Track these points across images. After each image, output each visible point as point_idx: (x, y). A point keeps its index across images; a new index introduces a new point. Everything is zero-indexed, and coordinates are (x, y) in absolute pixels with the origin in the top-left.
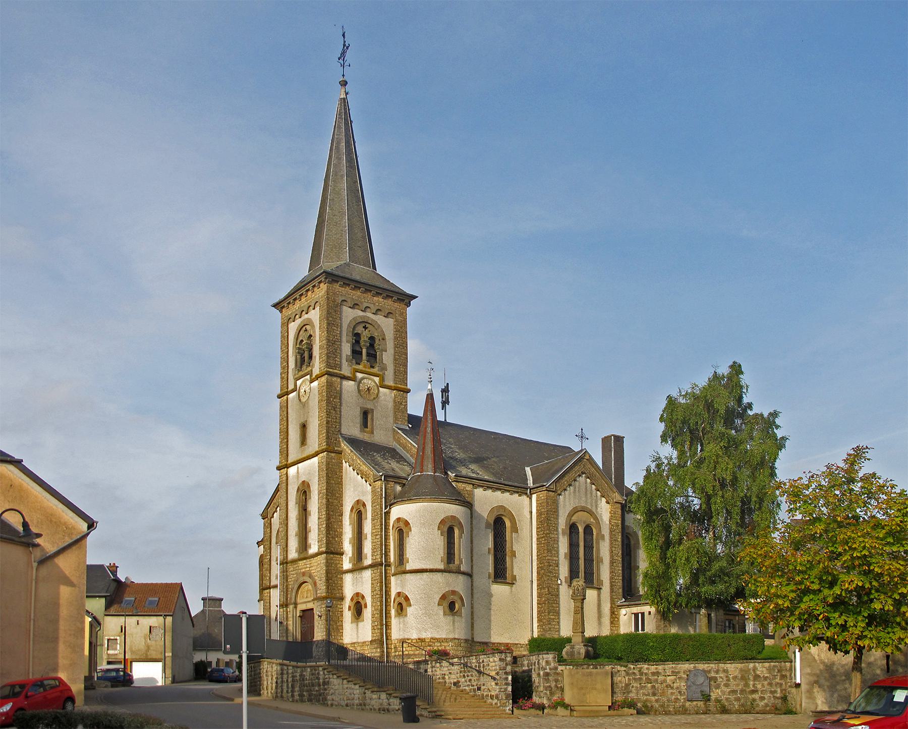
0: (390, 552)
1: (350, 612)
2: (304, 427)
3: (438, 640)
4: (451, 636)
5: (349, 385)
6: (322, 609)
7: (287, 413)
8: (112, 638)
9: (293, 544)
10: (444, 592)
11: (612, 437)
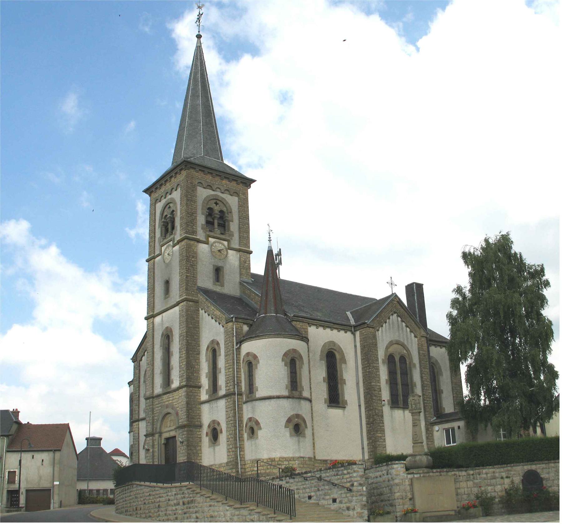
0: (241, 383)
1: (208, 438)
3: (286, 459)
4: (297, 455)
5: (203, 248)
6: (183, 436)
7: (154, 273)
8: (12, 470)
9: (158, 380)
10: (289, 416)
11: (414, 284)
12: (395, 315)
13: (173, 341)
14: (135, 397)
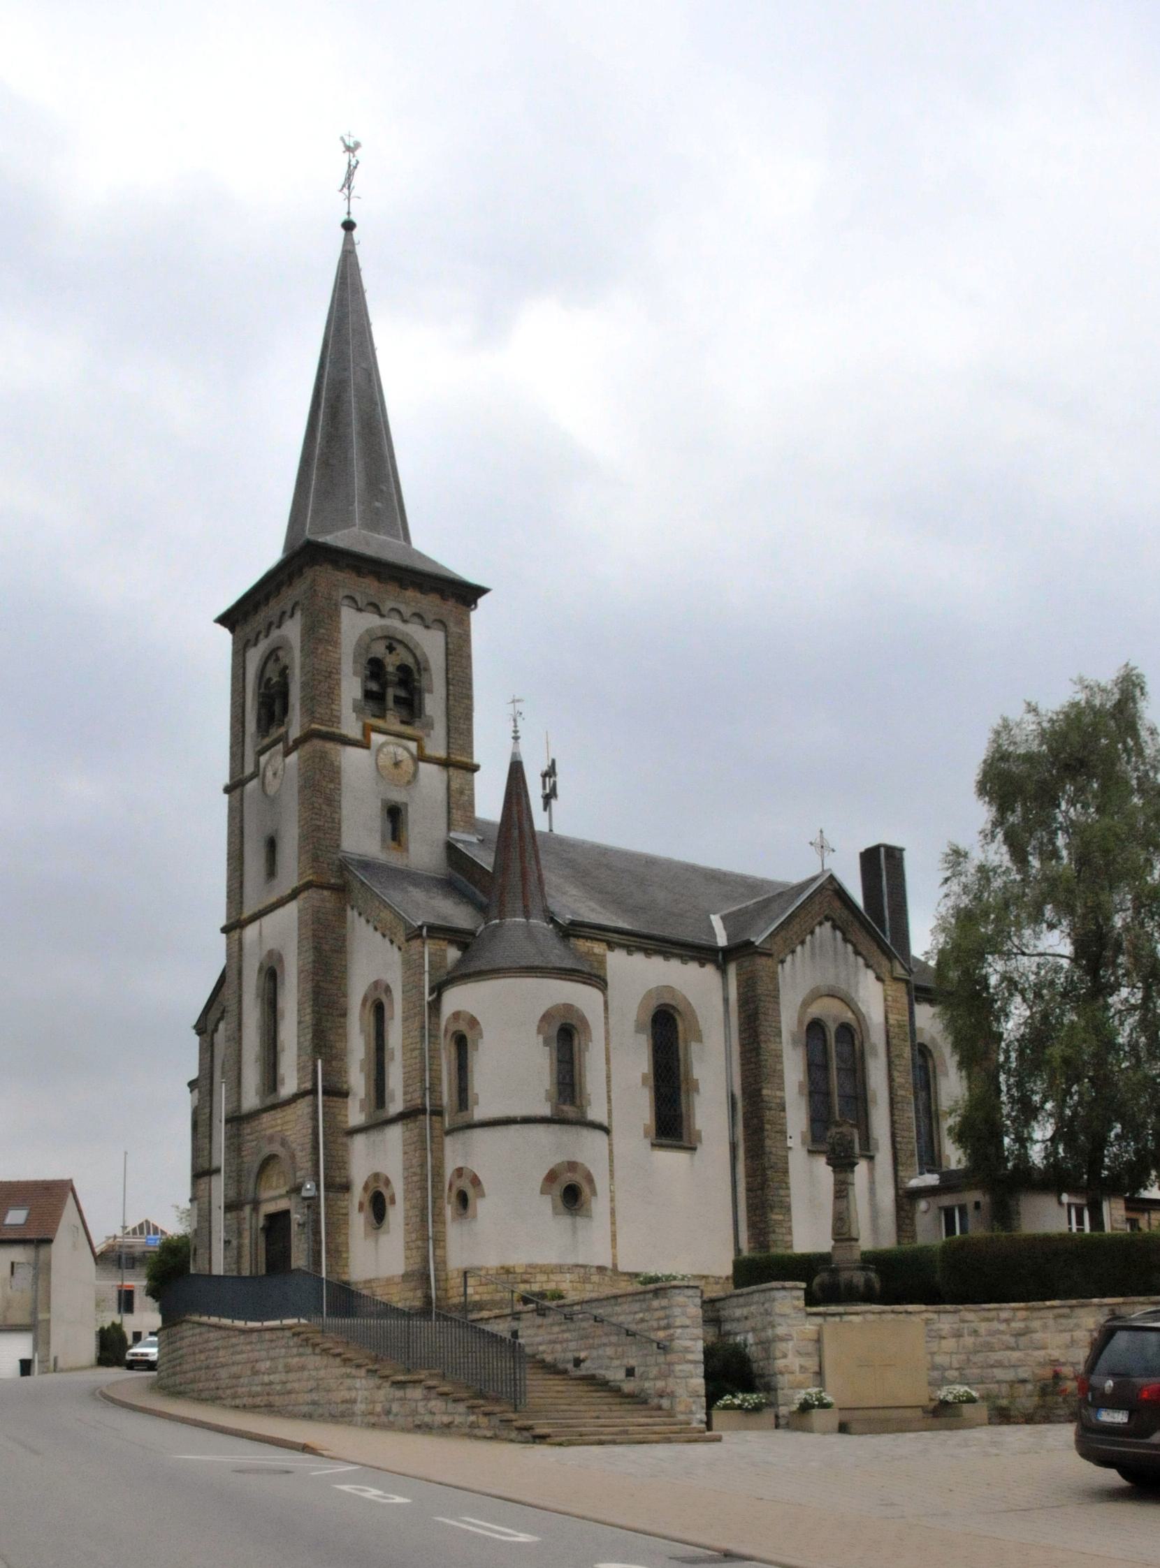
0: (440, 1084)
2: (272, 845)
4: (571, 1260)
10: (552, 1166)
11: (882, 850)
12: (828, 925)
13: (283, 984)
14: (203, 1117)
